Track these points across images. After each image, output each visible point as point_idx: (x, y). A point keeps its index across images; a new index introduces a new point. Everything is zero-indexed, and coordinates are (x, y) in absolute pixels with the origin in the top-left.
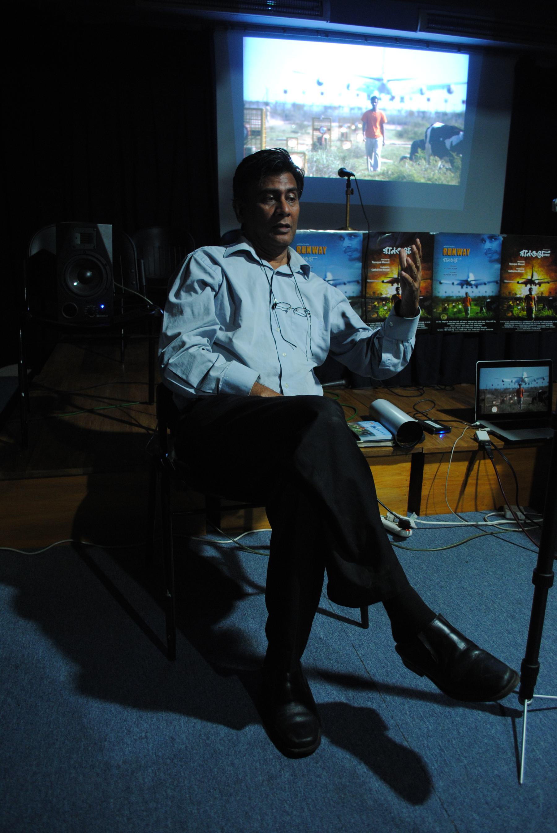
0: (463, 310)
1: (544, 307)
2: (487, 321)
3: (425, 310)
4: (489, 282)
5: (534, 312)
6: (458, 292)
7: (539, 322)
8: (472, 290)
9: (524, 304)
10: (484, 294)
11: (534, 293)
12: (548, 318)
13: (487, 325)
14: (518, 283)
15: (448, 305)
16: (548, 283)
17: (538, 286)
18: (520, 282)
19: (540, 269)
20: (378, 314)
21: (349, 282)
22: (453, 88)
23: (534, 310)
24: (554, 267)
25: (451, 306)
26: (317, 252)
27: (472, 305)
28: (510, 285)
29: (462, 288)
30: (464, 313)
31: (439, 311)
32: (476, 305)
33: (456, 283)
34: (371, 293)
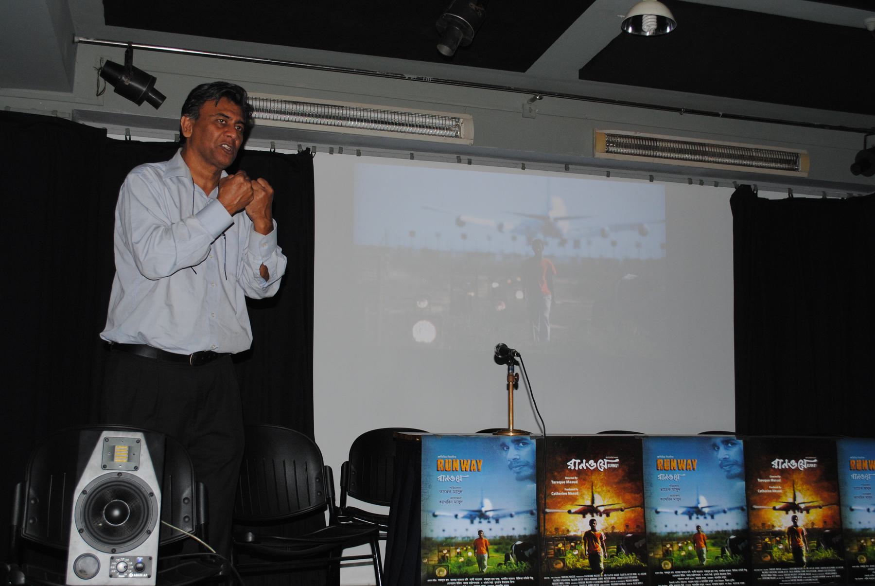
0: (475, 560)
2: (734, 570)
3: (636, 555)
5: (804, 552)
6: (683, 525)
7: (814, 570)
8: (706, 521)
9: (787, 542)
10: (726, 528)
11: (801, 524)
12: (826, 562)
14: (774, 508)
15: (866, 541)
16: (820, 507)
17: (604, 516)
18: (573, 511)
20: (564, 563)
21: (518, 513)
23: (804, 549)
24: (628, 485)
25: (676, 548)
26: (468, 468)
27: (708, 545)
28: (556, 517)
29: (690, 518)
30: (697, 559)
31: (433, 563)
32: (714, 545)
33: (680, 511)
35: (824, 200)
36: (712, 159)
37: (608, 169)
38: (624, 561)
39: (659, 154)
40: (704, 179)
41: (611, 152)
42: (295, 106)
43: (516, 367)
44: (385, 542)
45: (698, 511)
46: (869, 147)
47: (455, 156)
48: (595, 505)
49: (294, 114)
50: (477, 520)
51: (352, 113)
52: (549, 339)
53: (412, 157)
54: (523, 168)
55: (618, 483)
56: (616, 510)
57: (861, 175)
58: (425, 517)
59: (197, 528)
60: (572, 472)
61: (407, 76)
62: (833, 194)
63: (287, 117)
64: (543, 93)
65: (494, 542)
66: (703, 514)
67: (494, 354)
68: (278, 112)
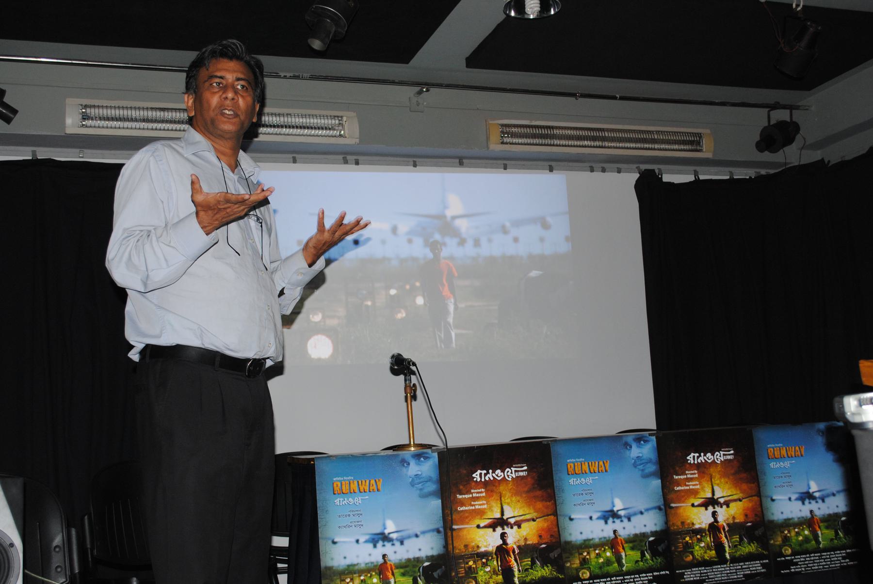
0: (614, 559)
1: (741, 540)
2: (655, 574)
4: (838, 492)
5: (727, 549)
6: (600, 531)
8: (623, 525)
10: (644, 530)
11: (721, 519)
12: (750, 557)
13: (848, 556)
17: (515, 527)
18: (696, 504)
19: (514, 499)
20: (693, 555)
21: (424, 533)
22: (549, 220)
23: (726, 546)
24: (744, 475)
27: (822, 528)
28: (681, 511)
30: (616, 565)
31: (575, 566)
32: (827, 528)
33: (362, 539)
34: (462, 547)
35: (732, 181)
36: (612, 145)
37: (505, 162)
38: (540, 575)
39: (557, 142)
40: (606, 165)
41: (507, 143)
42: (162, 113)
43: (413, 377)
44: (286, 576)
45: (384, 538)
46: (773, 122)
47: (341, 157)
48: (715, 497)
49: (163, 121)
50: (380, 543)
51: (121, 112)
52: (454, 345)
53: (295, 161)
54: (415, 165)
55: (734, 474)
56: (528, 520)
57: (766, 152)
58: (324, 546)
59: (71, 578)
60: (479, 484)
61: (282, 75)
62: (741, 174)
63: (155, 125)
64: (430, 85)
65: (399, 566)
66: (619, 517)
67: (389, 365)
68: (144, 120)
